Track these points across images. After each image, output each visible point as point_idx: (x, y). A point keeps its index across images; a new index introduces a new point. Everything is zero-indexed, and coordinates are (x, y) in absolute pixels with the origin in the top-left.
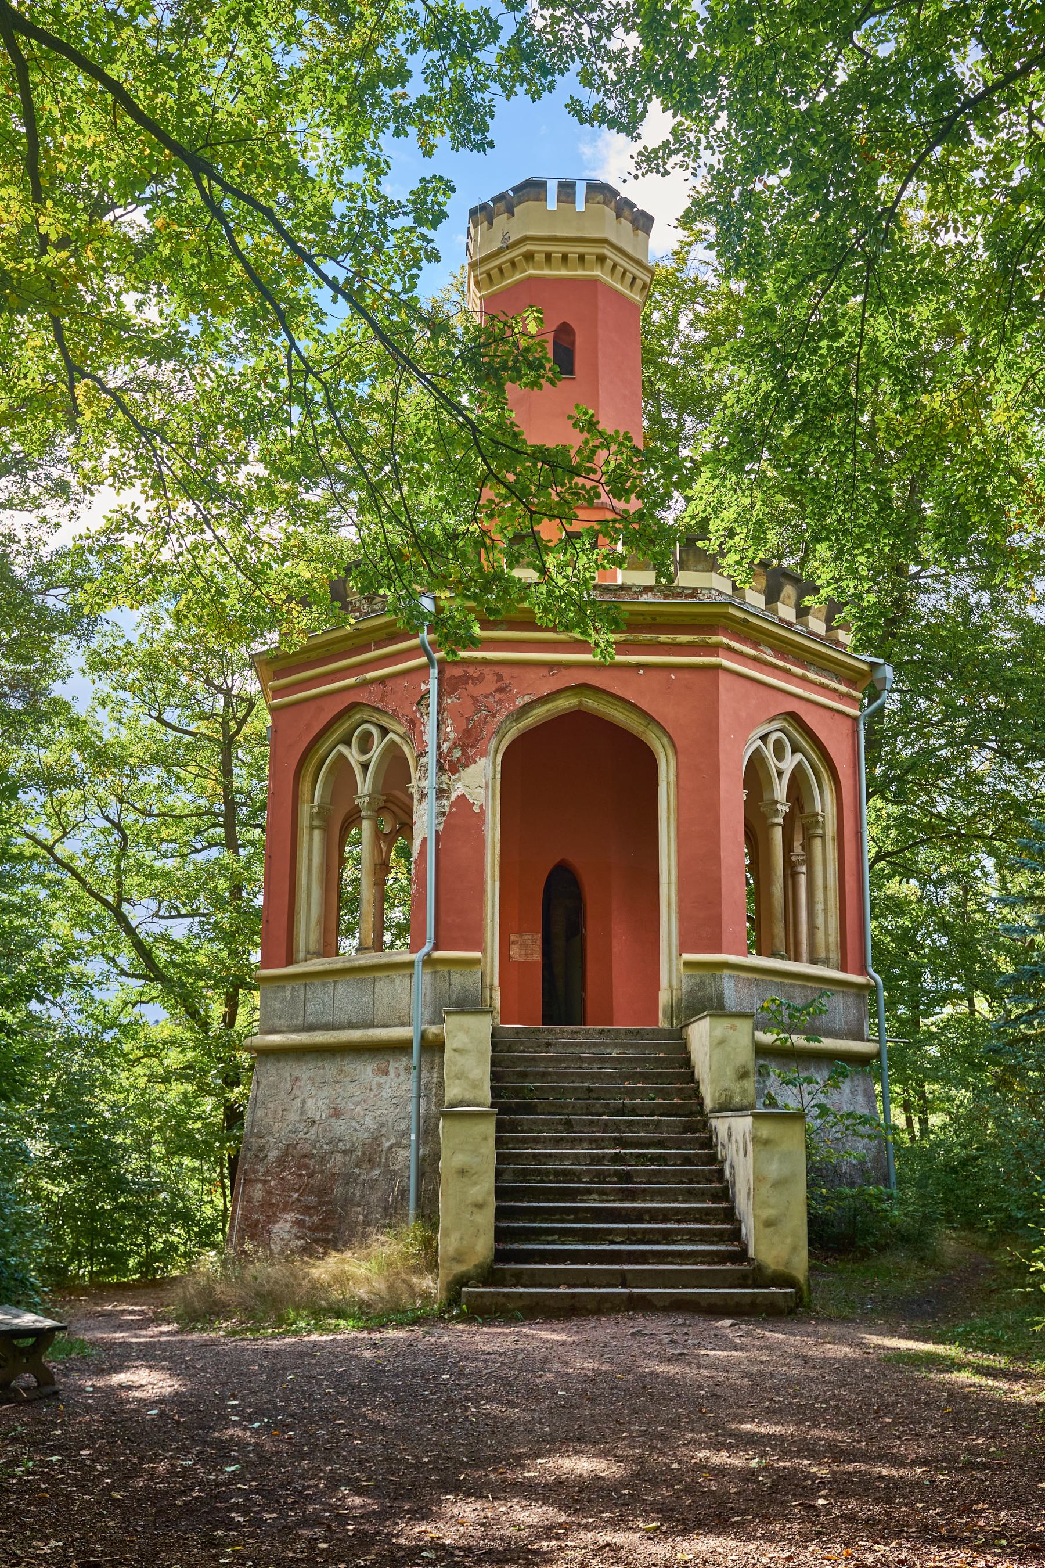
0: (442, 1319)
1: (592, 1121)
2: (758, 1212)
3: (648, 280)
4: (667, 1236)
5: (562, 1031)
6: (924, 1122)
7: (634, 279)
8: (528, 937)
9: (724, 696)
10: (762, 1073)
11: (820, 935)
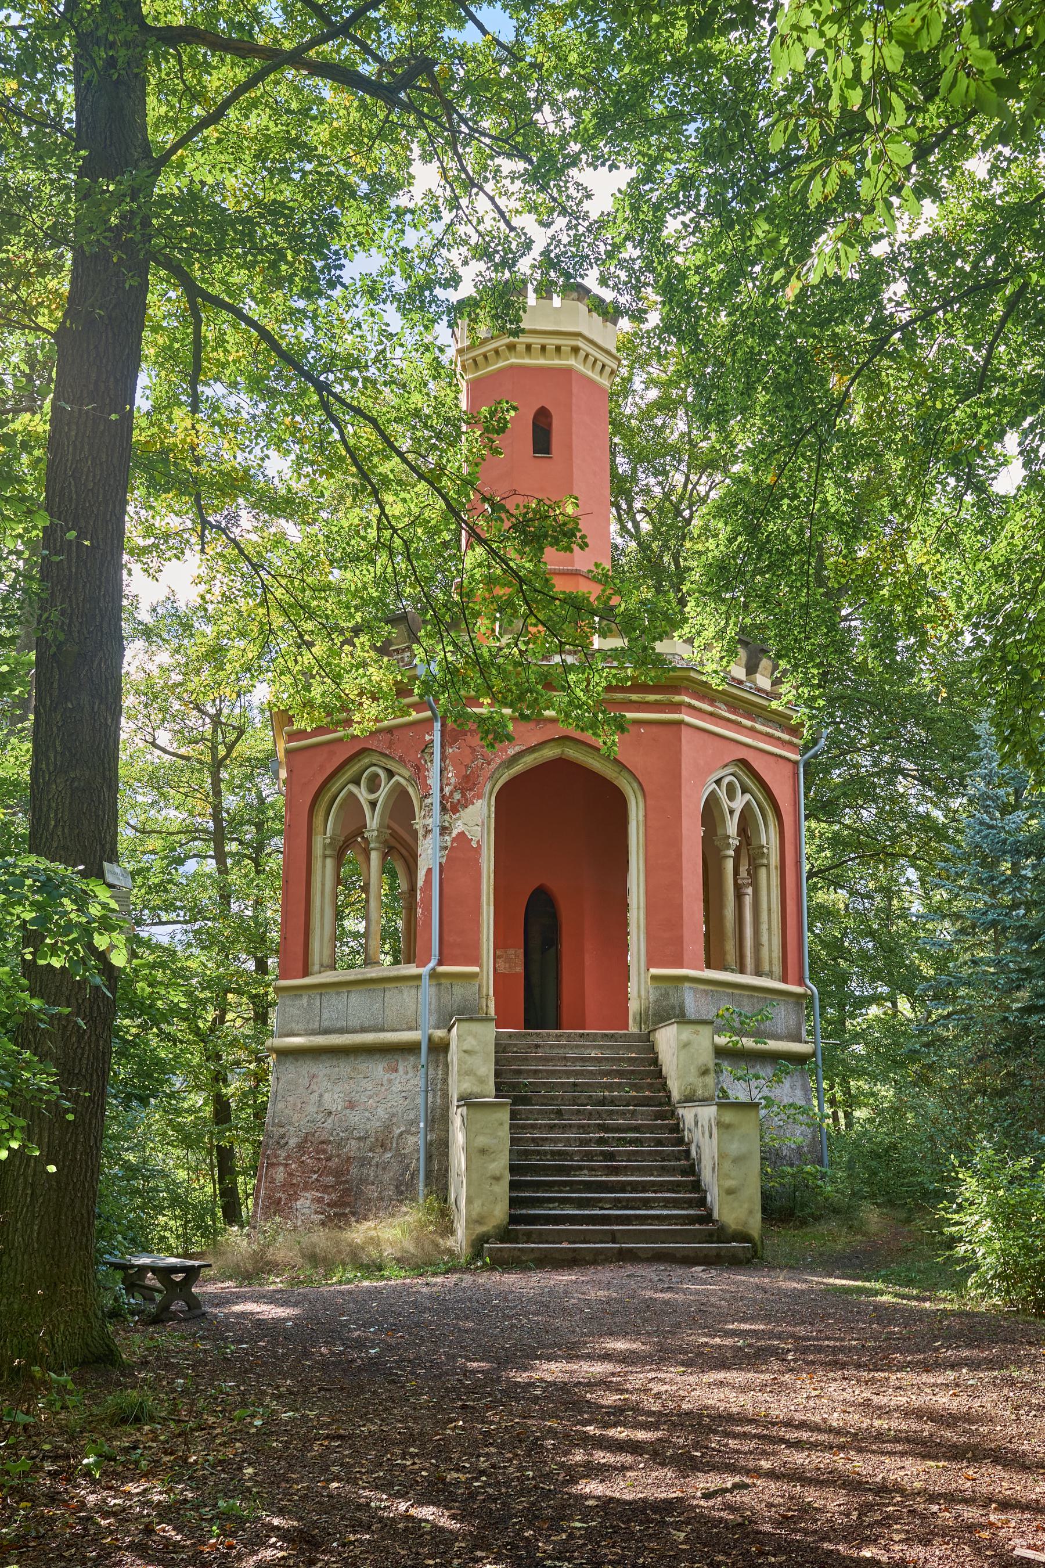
0: (468, 1269)
1: (579, 1111)
2: (722, 1182)
3: (615, 367)
4: (646, 1203)
5: (548, 1035)
6: (848, 1115)
7: (604, 366)
8: (512, 951)
9: (685, 747)
10: (718, 1070)
11: (765, 952)
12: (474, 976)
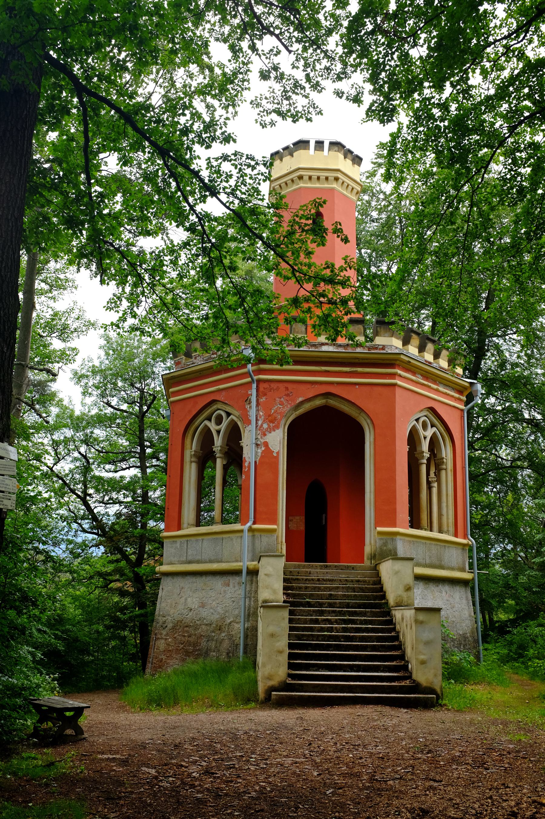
7: (353, 189)
12: (274, 531)
